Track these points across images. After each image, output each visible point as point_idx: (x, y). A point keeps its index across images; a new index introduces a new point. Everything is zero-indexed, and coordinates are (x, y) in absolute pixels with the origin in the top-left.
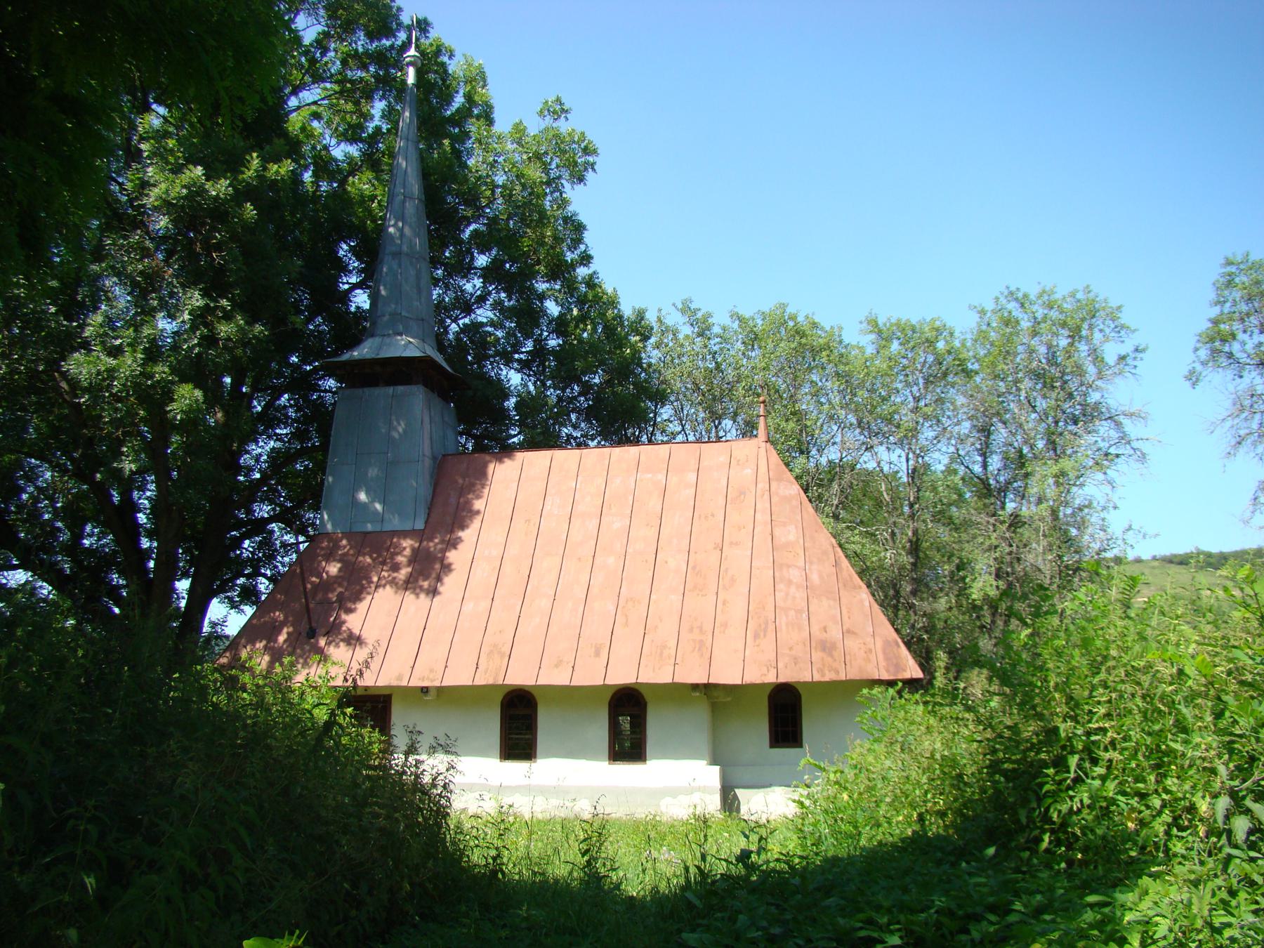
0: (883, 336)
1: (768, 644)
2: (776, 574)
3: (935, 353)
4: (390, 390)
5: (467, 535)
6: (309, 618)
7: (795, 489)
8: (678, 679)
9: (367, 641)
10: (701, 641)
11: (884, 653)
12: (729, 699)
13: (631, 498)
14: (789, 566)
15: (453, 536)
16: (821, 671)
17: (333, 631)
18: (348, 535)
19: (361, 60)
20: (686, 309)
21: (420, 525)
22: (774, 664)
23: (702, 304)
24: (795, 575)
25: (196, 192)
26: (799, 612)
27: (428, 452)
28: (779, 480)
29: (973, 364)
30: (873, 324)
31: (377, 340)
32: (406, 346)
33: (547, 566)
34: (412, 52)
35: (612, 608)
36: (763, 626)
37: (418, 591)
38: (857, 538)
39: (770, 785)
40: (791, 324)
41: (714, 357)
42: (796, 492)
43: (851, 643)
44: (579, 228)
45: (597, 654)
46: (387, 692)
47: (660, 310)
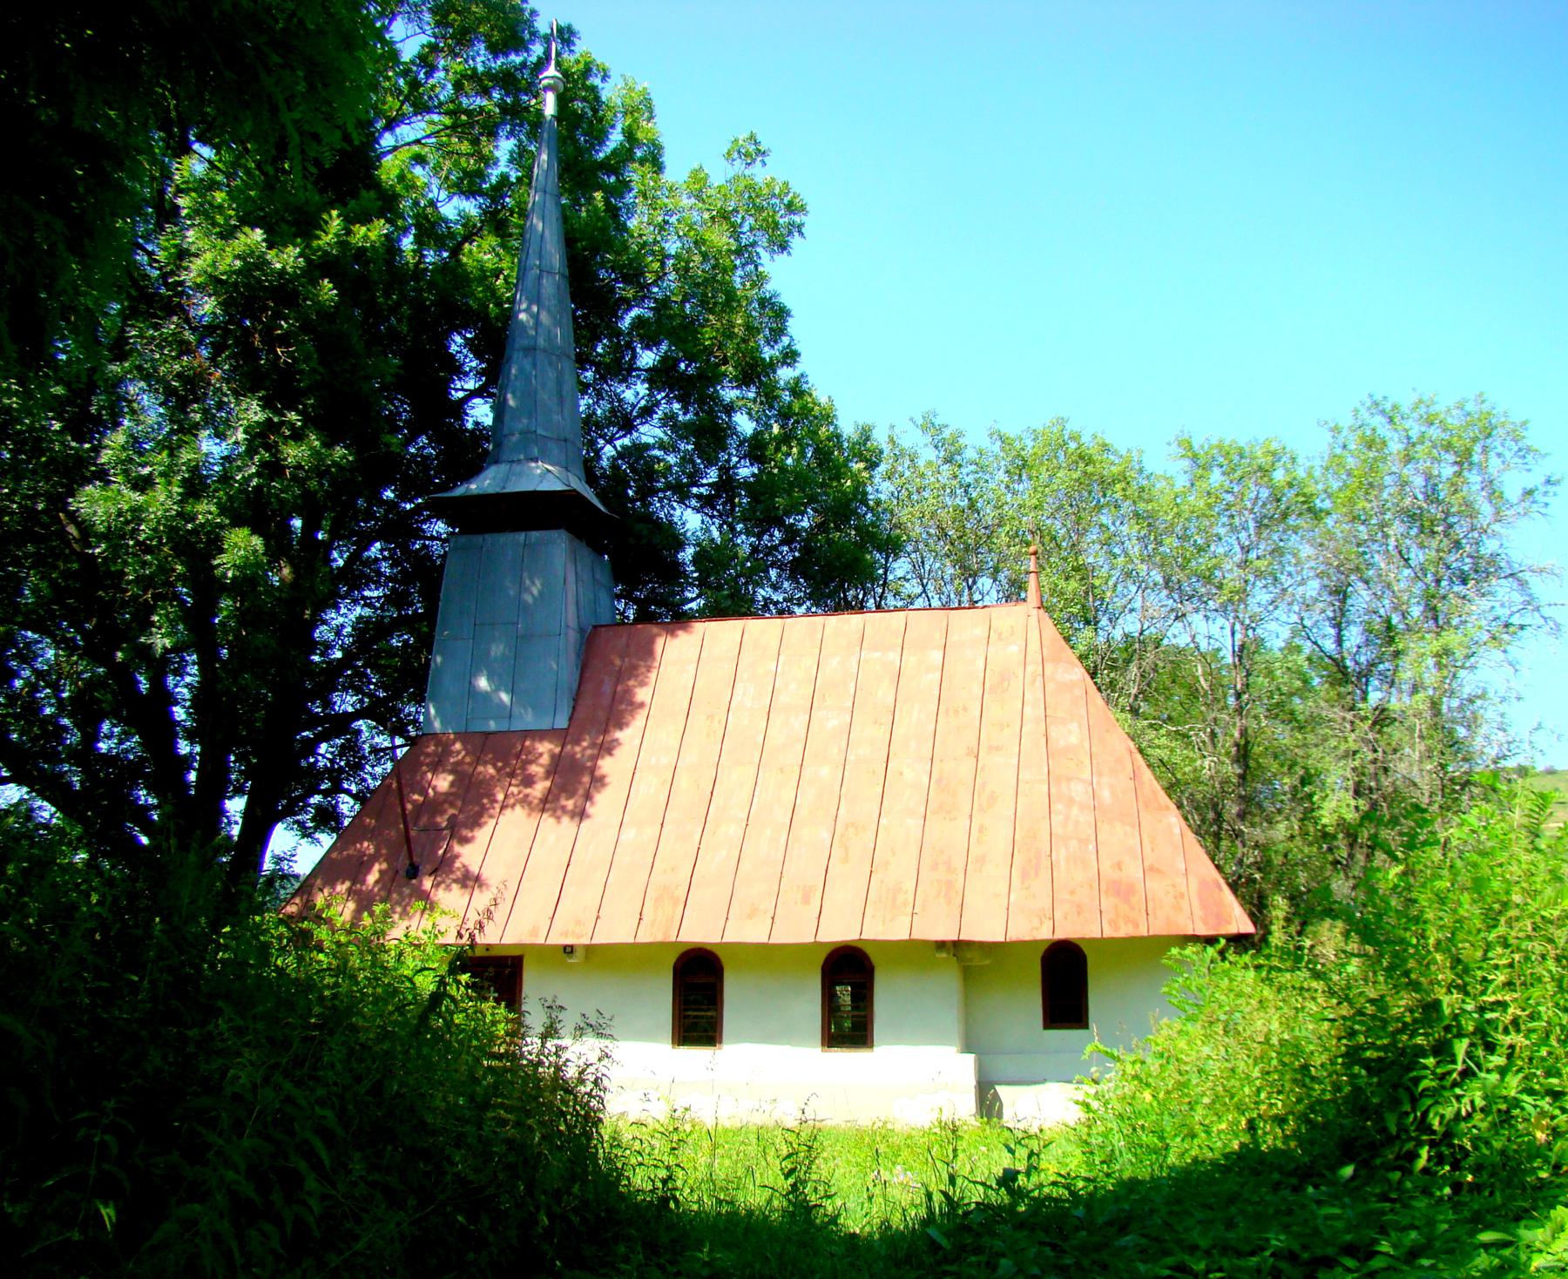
0: (1200, 463)
1: (1041, 885)
2: (1053, 790)
5: (627, 736)
7: (1079, 673)
8: (915, 936)
11: (1201, 899)
13: (853, 684)
14: (1069, 779)
15: (608, 738)
17: (442, 867)
18: (463, 736)
19: (479, 82)
20: (929, 426)
21: (562, 722)
23: (952, 419)
24: (1078, 791)
25: (254, 264)
27: (573, 623)
32: (542, 476)
33: (736, 778)
34: (552, 71)
35: (827, 837)
37: (559, 813)
39: (1044, 1081)
40: (1072, 446)
43: (1156, 886)
44: (781, 314)
45: (806, 899)
46: (516, 953)
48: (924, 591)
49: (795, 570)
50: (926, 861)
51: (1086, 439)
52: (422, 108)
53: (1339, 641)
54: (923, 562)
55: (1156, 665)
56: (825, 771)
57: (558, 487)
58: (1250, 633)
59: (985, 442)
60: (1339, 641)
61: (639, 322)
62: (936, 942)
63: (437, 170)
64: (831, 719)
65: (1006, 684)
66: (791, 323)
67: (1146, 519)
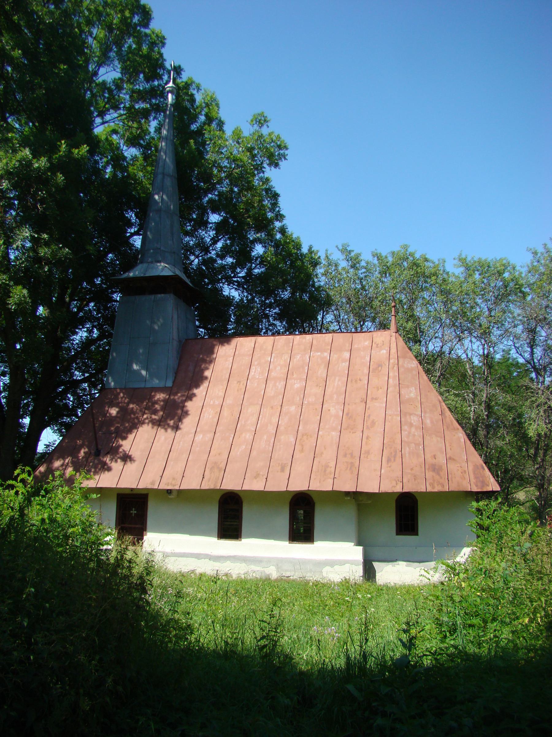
0: (469, 268)
1: (396, 466)
2: (402, 419)
3: (503, 280)
4: (152, 297)
5: (200, 392)
6: (97, 444)
7: (415, 363)
8: (336, 488)
9: (135, 459)
10: (352, 463)
11: (474, 473)
12: (370, 502)
13: (307, 368)
14: (411, 414)
15: (191, 392)
16: (432, 485)
17: (114, 452)
18: (126, 390)
19: (141, 96)
20: (346, 251)
21: (169, 384)
22: (401, 479)
23: (355, 248)
24: (415, 420)
25: (26, 165)
26: (417, 445)
28: (404, 357)
29: (525, 288)
30: (463, 261)
31: (145, 265)
32: (163, 269)
33: (251, 411)
34: (171, 84)
35: (293, 440)
36: (393, 454)
37: (166, 427)
38: (452, 397)
39: (396, 560)
40: (411, 258)
41: (361, 282)
42: (415, 365)
43: (452, 467)
44: (276, 196)
45: (283, 470)
46: (145, 492)
47: (327, 250)
48: (340, 328)
49: (280, 317)
50: (341, 452)
51: (417, 256)
52: (116, 108)
53: (532, 353)
54: (339, 315)
55: (449, 362)
56: (293, 408)
57: (170, 273)
58: (491, 349)
59: (369, 258)
60: (532, 353)
61: (211, 201)
62: (345, 492)
63: (123, 136)
64: (297, 384)
65: (380, 368)
66: (280, 199)
67: (446, 293)
